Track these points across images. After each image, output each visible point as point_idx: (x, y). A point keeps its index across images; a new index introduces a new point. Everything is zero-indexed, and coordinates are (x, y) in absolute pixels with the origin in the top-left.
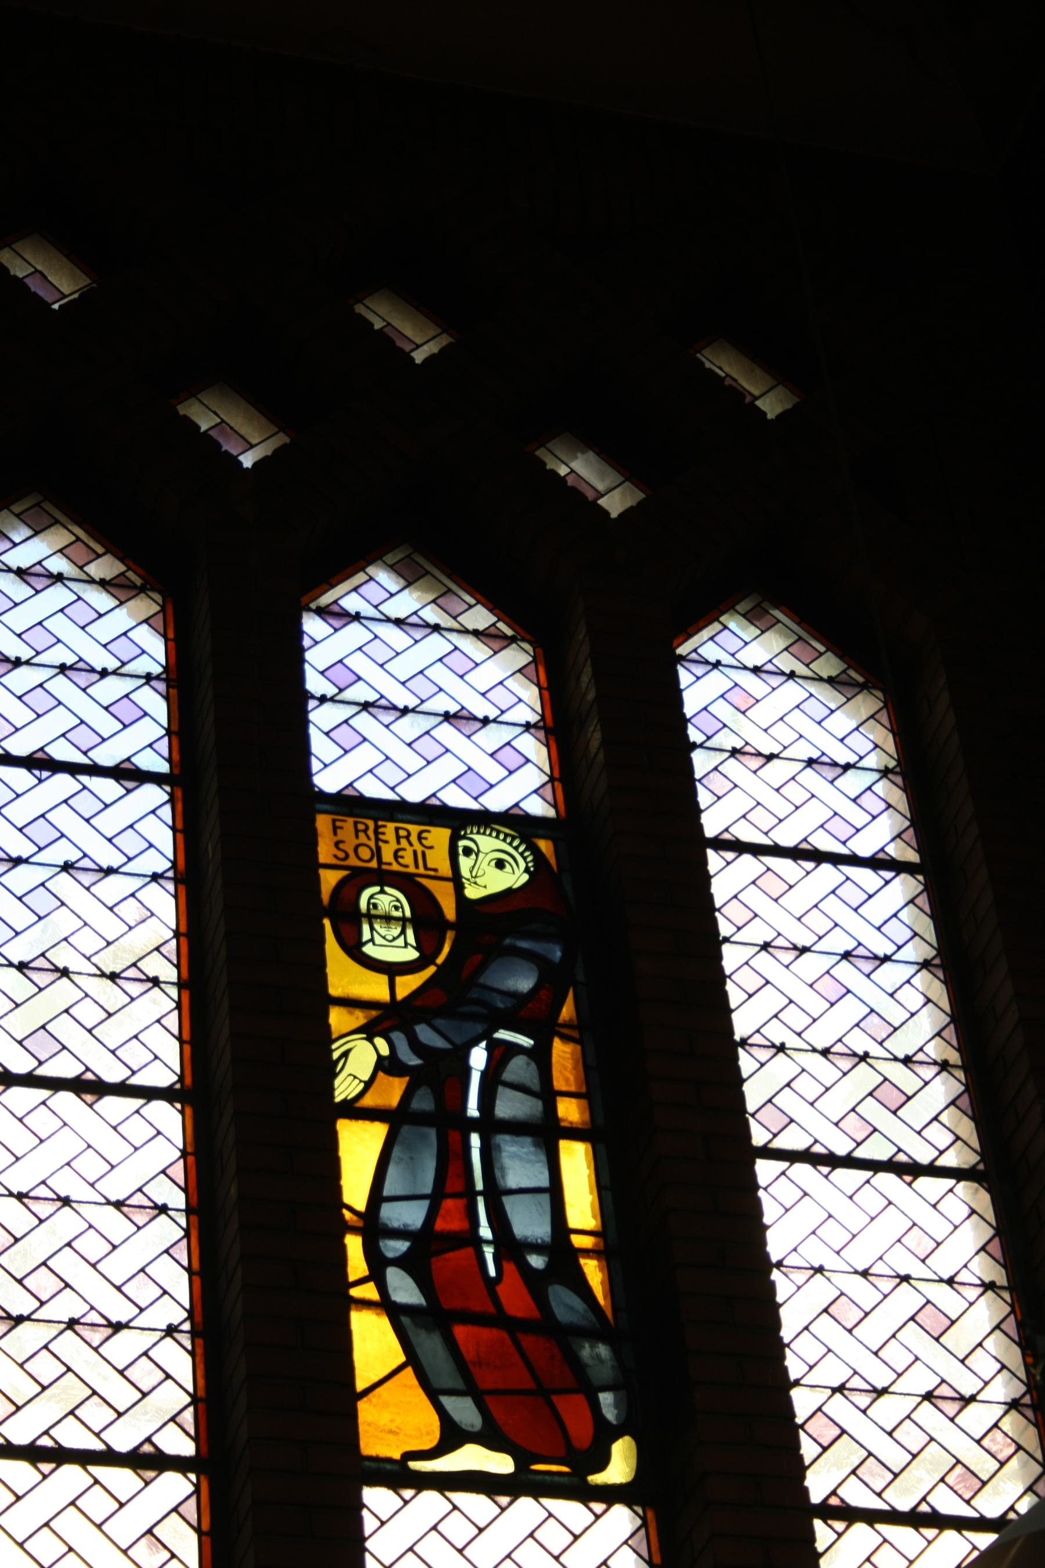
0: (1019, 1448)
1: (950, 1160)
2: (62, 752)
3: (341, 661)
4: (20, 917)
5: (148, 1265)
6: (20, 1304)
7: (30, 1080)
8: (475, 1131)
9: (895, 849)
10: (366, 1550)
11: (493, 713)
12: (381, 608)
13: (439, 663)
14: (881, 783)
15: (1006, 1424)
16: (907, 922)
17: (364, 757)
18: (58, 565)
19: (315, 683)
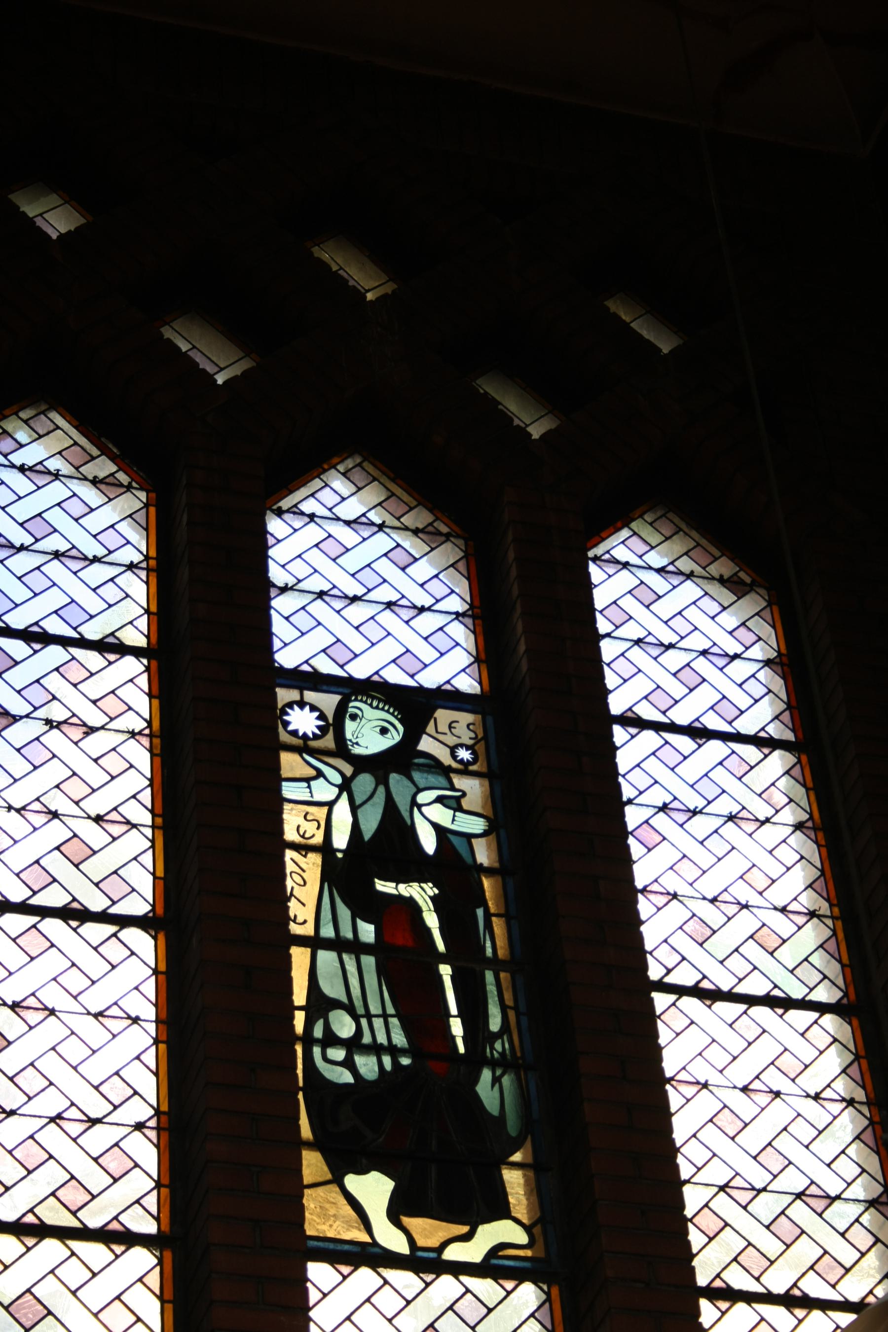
1: (822, 994)
2: (55, 627)
5: (121, 1139)
7: (24, 908)
10: (310, 1319)
12: (334, 510)
13: (384, 558)
14: (762, 671)
15: (865, 1219)
19: (277, 575)
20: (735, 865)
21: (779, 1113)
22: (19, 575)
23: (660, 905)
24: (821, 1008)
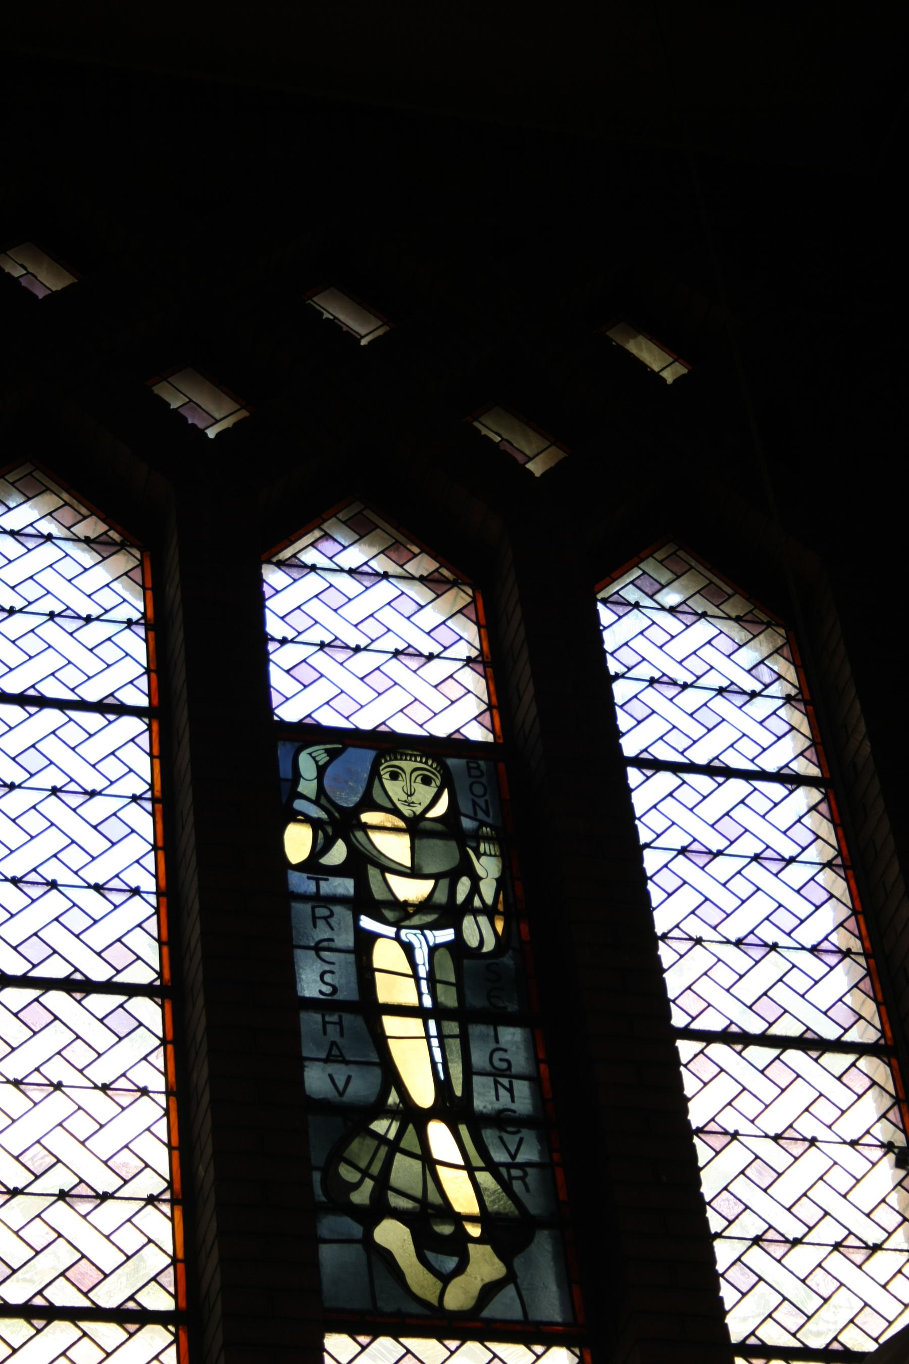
0: (874, 1083)
2: (52, 690)
3: (304, 661)
4: (15, 837)
6: (14, 775)
7: (24, 981)
8: (432, 1018)
9: (839, 939)
11: (290, 634)
13: (388, 607)
15: (820, 878)
16: (897, 1208)
17: (321, 691)
18: (47, 527)
19: (274, 627)
20: (760, 906)
21: (814, 1162)
22: (90, 647)
23: (833, 964)
24: (860, 1049)
